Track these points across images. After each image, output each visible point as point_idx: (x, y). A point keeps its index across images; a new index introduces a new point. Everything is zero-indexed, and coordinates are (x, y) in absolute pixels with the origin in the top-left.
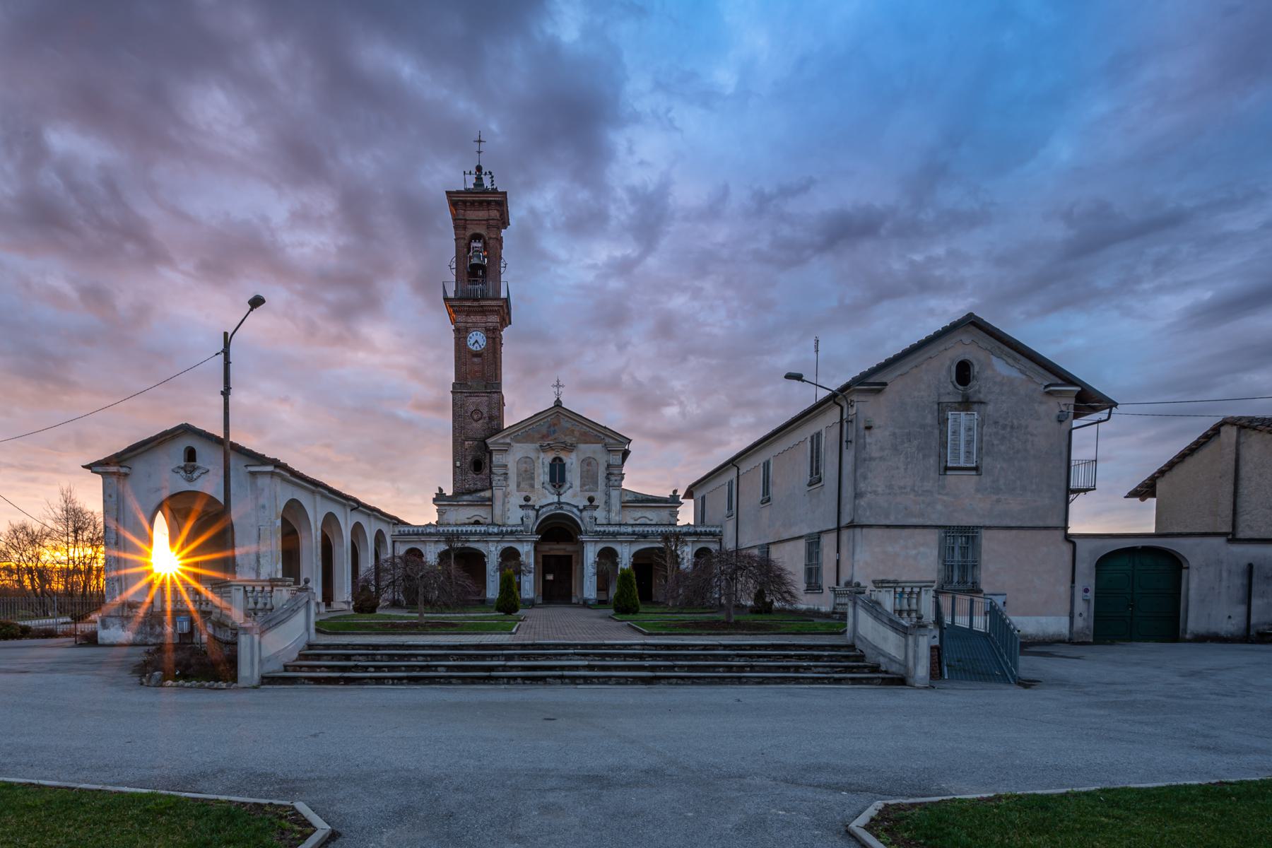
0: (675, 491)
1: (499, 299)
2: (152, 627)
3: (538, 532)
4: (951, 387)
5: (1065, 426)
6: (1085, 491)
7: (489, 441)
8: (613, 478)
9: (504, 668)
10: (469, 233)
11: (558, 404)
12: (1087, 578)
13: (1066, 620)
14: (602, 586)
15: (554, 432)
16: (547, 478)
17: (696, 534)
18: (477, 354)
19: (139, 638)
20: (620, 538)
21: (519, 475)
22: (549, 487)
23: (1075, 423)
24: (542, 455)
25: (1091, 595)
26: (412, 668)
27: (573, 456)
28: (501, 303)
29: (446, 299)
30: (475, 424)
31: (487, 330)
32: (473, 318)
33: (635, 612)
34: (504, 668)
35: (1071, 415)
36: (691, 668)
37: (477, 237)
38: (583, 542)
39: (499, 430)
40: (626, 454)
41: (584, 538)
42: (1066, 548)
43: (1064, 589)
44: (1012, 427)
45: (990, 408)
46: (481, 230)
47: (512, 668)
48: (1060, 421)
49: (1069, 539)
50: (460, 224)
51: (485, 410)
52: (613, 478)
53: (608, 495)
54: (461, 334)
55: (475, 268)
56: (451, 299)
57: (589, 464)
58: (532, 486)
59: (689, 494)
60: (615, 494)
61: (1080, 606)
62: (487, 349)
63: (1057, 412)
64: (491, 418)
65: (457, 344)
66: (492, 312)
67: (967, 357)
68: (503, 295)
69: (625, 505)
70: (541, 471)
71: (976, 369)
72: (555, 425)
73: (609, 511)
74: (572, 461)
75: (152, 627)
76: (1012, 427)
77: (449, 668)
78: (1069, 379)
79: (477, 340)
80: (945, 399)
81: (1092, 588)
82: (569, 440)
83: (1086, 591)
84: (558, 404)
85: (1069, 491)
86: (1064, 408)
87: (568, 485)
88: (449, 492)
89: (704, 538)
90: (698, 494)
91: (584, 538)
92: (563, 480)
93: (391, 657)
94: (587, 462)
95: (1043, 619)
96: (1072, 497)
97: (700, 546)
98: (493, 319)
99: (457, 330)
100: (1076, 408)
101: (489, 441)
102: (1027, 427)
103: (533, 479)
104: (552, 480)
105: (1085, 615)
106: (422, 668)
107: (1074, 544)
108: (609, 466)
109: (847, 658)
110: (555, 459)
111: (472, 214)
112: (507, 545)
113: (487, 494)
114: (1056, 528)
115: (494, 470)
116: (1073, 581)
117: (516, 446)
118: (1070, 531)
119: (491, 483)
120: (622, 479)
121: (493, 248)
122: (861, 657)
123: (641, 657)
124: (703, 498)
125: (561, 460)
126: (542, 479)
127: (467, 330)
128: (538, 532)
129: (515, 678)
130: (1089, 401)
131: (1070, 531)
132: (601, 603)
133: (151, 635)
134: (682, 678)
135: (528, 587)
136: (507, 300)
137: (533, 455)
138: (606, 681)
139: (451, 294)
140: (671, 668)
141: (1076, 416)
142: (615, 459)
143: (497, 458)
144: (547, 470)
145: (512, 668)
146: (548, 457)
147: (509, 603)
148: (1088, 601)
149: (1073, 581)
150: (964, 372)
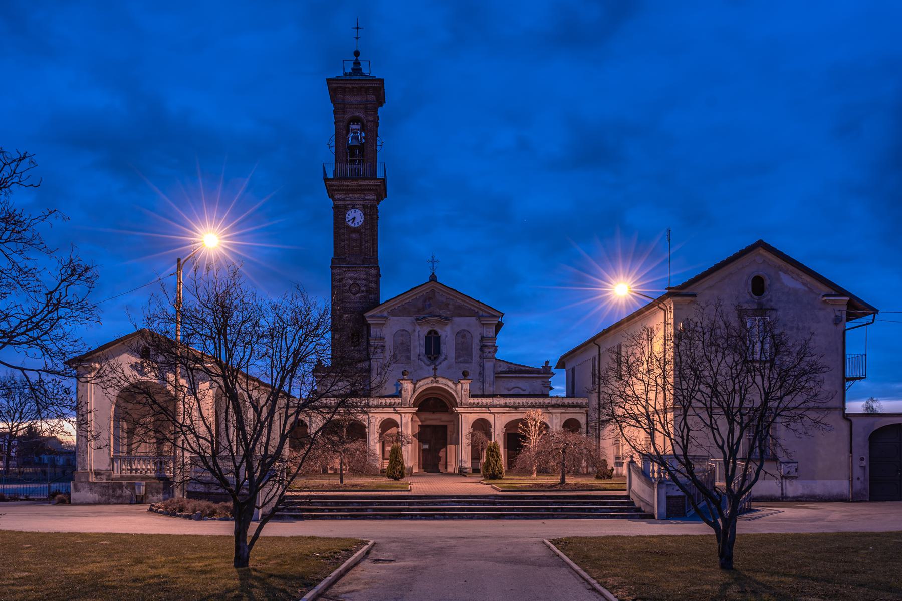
0: (547, 362)
1: (376, 179)
2: (114, 490)
3: (415, 405)
4: (748, 297)
5: (840, 328)
6: (860, 378)
7: (367, 315)
8: (486, 350)
9: (409, 510)
10: (348, 116)
11: (433, 278)
12: (862, 449)
13: (846, 483)
14: (475, 457)
15: (430, 305)
16: (423, 350)
17: (563, 406)
18: (355, 230)
19: (104, 499)
20: (493, 410)
21: (396, 348)
22: (425, 358)
23: (848, 325)
24: (418, 328)
25: (866, 463)
26: (352, 510)
27: (448, 328)
28: (378, 183)
29: (326, 179)
30: (353, 298)
31: (365, 208)
32: (351, 196)
33: (500, 479)
34: (409, 510)
35: (844, 319)
36: (524, 510)
37: (356, 120)
38: (458, 414)
39: (376, 304)
40: (499, 326)
41: (459, 410)
42: (844, 425)
43: (844, 457)
44: (798, 329)
45: (780, 313)
46: (361, 114)
47: (413, 510)
48: (836, 324)
49: (847, 417)
50: (339, 109)
51: (363, 284)
52: (486, 350)
53: (482, 367)
54: (339, 212)
55: (352, 149)
56: (331, 179)
57: (463, 336)
58: (409, 358)
59: (561, 364)
60: (489, 365)
61: (858, 472)
62: (364, 225)
63: (833, 316)
64: (369, 292)
65: (336, 221)
66: (369, 190)
67: (760, 274)
68: (380, 175)
69: (498, 375)
70: (417, 343)
71: (767, 283)
72: (430, 299)
73: (483, 383)
74: (447, 333)
75: (114, 490)
76: (798, 329)
77: (374, 510)
78: (842, 292)
79: (356, 218)
80: (745, 306)
81: (867, 457)
82: (443, 313)
83: (862, 459)
84: (433, 278)
85: (845, 379)
86: (838, 313)
87: (443, 357)
88: (328, 362)
89: (571, 410)
90: (569, 366)
91: (459, 410)
92: (438, 351)
93: (337, 504)
94: (461, 334)
95: (828, 483)
96: (847, 384)
97: (568, 416)
98: (371, 196)
99: (336, 208)
100: (848, 314)
101: (367, 315)
102: (809, 328)
103: (409, 350)
104: (428, 351)
105: (862, 479)
106: (358, 510)
107: (850, 421)
108: (482, 337)
109: (623, 503)
110: (430, 332)
111: (350, 98)
112: (387, 416)
113: (365, 365)
114: (836, 408)
115: (372, 342)
116: (851, 452)
117: (393, 320)
118: (847, 412)
119: (368, 355)
120: (496, 350)
121: (371, 127)
122: (633, 503)
123: (494, 504)
124: (573, 369)
125: (436, 332)
126: (417, 351)
127: (346, 208)
128: (415, 405)
129: (416, 515)
130: (857, 308)
131: (847, 412)
132: (476, 471)
133: (113, 496)
134: (518, 515)
135: (410, 455)
136: (384, 181)
137: (409, 328)
138: (471, 517)
139: (331, 175)
140: (512, 510)
141: (848, 320)
142: (490, 332)
143: (373, 331)
144: (423, 342)
145: (413, 510)
146: (424, 330)
147: (397, 471)
148: (864, 468)
149: (851, 452)
150: (758, 286)
